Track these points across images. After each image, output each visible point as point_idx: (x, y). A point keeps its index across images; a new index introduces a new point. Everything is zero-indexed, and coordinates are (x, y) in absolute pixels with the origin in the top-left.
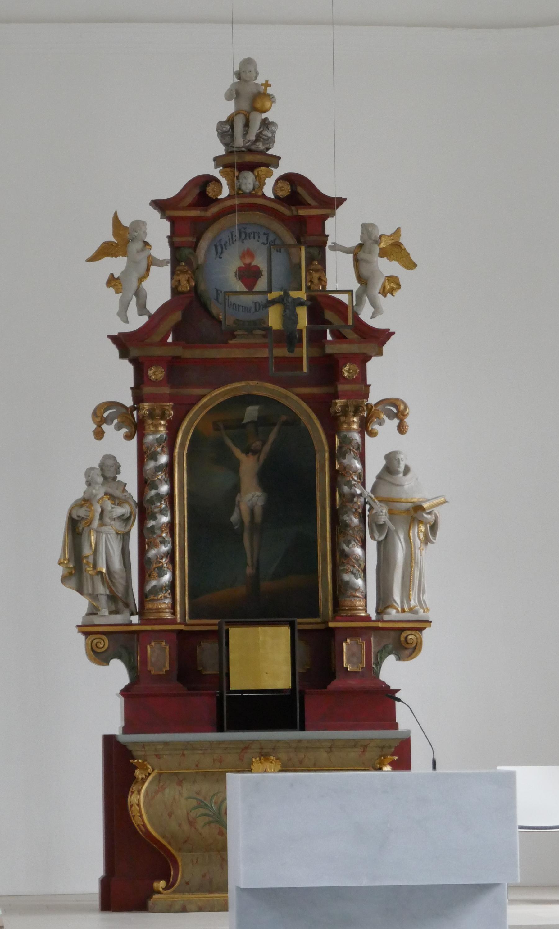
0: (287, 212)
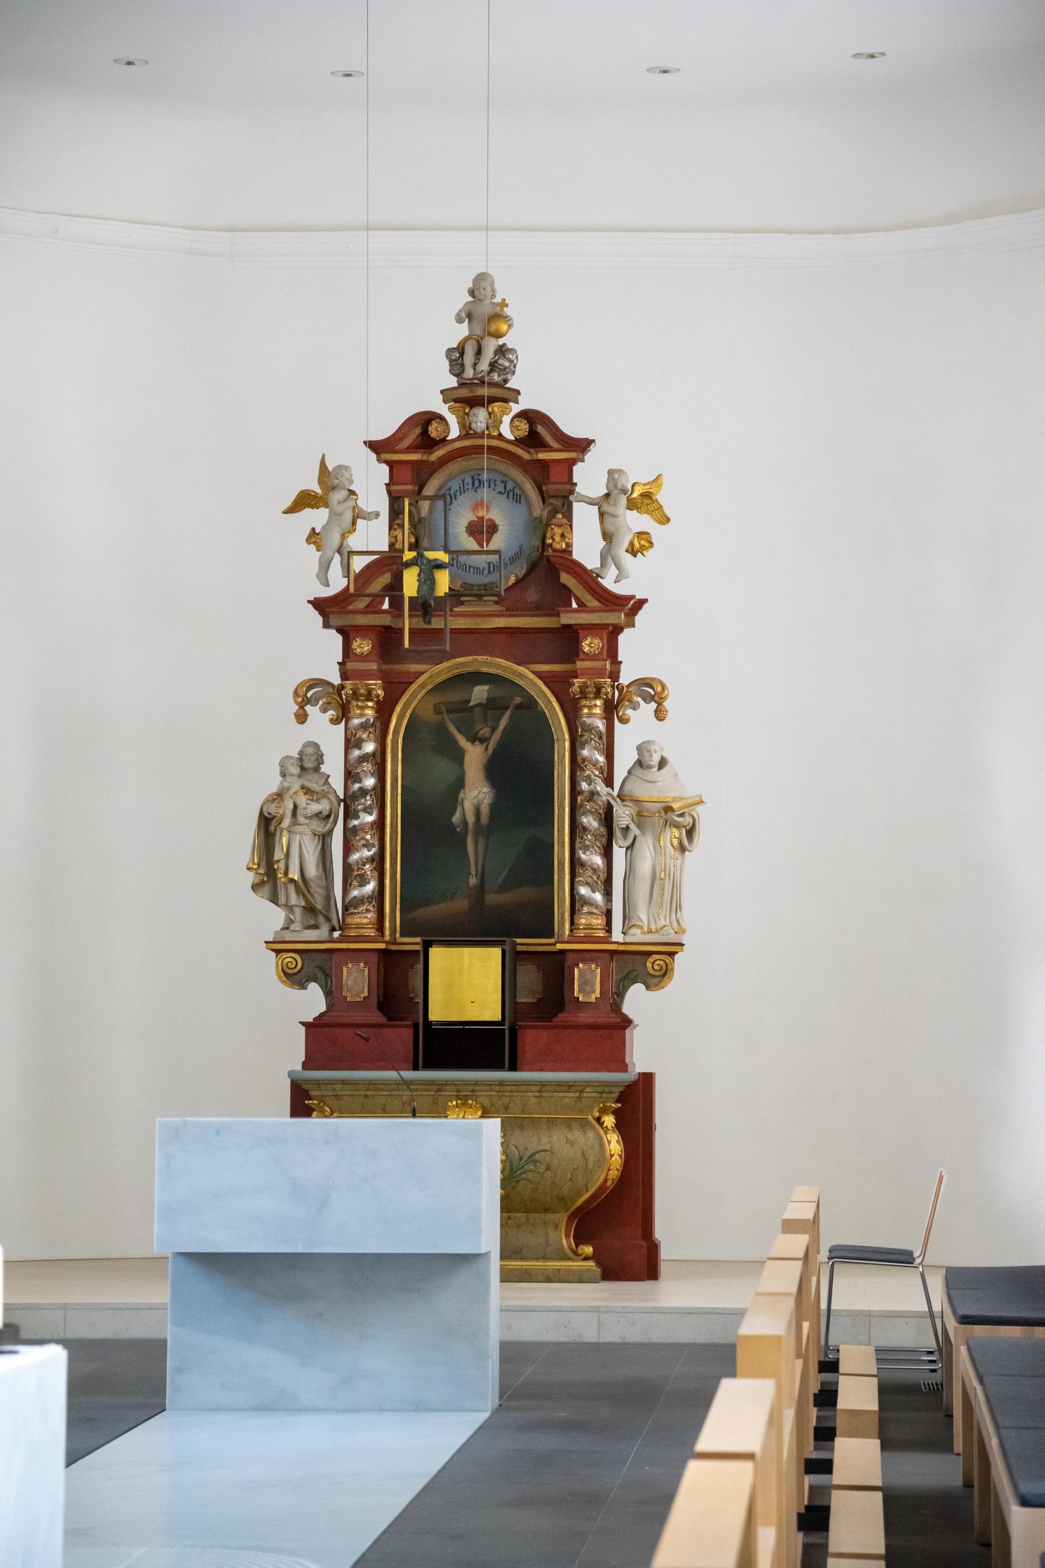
0: (526, 456)
